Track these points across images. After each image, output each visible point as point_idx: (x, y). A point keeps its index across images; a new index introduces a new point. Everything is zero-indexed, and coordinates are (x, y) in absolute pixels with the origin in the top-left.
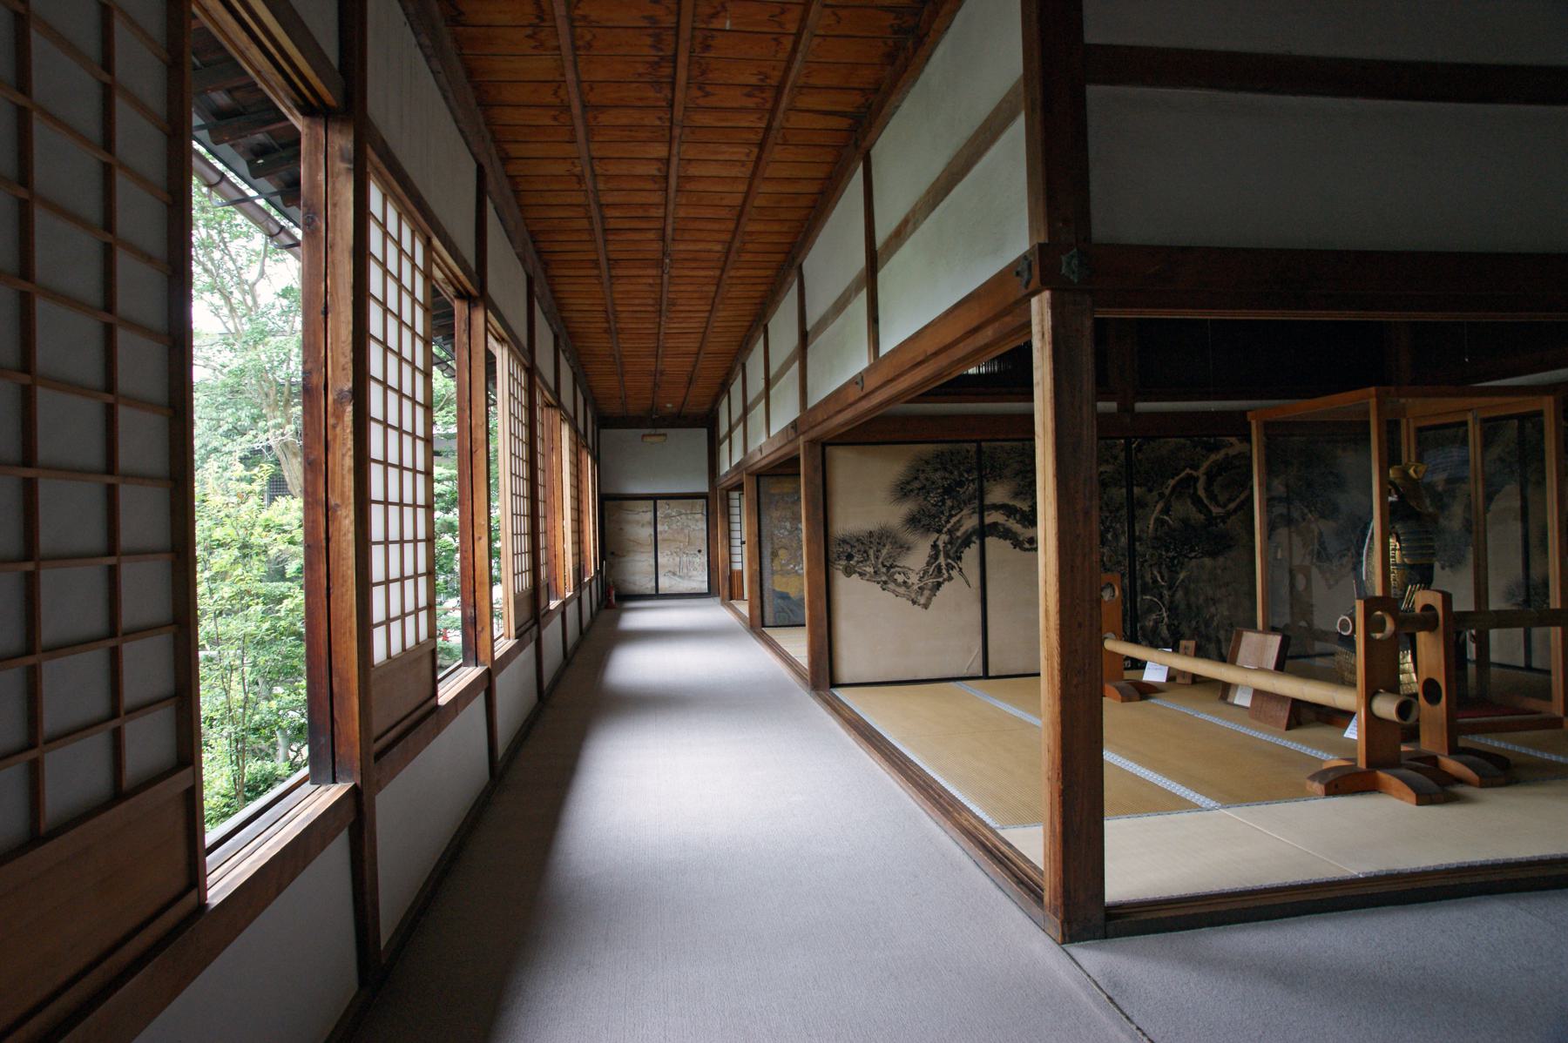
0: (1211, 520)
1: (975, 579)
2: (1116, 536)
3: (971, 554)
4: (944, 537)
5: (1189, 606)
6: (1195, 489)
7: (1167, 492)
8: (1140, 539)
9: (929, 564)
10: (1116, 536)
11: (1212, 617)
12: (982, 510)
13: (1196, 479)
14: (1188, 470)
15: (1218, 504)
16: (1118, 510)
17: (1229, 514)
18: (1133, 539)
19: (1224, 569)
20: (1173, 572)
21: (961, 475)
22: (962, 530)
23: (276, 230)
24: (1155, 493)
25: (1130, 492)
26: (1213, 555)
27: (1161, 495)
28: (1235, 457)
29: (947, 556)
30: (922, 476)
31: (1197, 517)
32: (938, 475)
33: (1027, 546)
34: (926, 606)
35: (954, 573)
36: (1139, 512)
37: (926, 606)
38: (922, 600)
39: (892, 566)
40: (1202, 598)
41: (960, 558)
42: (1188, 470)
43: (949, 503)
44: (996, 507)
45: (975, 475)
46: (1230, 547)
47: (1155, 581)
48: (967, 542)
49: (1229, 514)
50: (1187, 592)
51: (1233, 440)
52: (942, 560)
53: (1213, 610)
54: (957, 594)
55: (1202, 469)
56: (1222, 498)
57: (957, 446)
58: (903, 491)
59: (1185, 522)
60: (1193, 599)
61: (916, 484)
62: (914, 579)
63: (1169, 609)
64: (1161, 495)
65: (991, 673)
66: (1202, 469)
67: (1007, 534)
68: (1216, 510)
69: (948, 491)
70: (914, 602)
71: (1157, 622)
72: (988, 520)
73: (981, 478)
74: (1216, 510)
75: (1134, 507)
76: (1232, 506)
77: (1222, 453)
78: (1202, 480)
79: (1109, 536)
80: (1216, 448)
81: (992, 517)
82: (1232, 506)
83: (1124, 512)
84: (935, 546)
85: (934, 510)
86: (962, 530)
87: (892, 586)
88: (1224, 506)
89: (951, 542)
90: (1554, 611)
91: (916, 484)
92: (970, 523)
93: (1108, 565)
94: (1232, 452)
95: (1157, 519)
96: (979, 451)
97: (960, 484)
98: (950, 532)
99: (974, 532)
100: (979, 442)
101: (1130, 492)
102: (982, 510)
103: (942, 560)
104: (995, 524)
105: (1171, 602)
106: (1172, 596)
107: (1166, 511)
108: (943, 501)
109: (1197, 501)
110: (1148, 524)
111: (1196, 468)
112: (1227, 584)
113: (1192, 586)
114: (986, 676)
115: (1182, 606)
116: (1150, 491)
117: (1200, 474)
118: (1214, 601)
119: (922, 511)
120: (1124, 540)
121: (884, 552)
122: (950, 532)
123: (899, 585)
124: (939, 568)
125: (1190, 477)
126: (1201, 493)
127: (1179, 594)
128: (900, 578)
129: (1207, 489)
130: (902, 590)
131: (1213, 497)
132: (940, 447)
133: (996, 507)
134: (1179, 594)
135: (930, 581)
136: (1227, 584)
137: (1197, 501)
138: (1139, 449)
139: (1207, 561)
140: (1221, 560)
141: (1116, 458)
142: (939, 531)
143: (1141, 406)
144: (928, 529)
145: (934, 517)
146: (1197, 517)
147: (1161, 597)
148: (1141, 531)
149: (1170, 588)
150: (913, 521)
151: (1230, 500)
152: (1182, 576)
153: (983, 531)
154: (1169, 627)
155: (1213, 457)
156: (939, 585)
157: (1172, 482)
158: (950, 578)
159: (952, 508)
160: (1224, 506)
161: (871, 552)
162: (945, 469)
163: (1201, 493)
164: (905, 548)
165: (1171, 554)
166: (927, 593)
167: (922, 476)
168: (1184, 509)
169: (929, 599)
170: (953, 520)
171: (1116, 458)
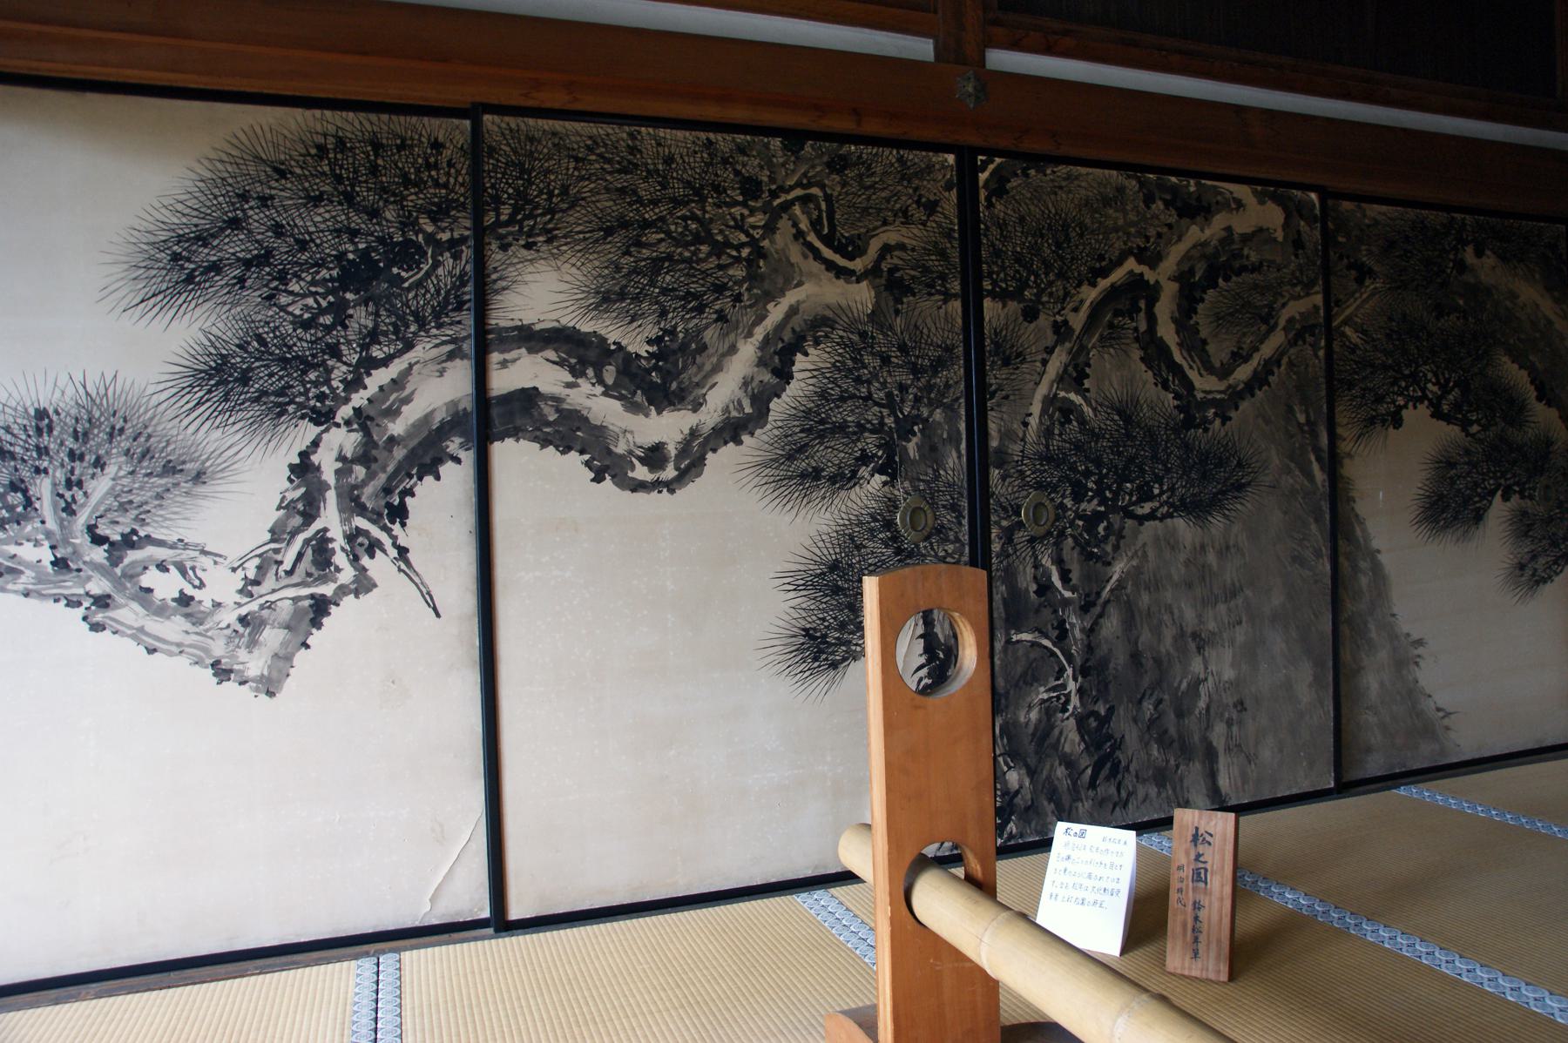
0: (1190, 411)
1: (459, 595)
2: (932, 451)
3: (441, 501)
4: (341, 440)
5: (1135, 657)
6: (1152, 319)
7: (1077, 321)
8: (1002, 459)
9: (276, 533)
10: (932, 451)
11: (1197, 683)
12: (484, 345)
13: (1152, 293)
14: (1131, 264)
15: (1208, 367)
16: (938, 365)
17: (1237, 395)
18: (980, 459)
19: (1224, 551)
20: (1094, 558)
21: (407, 223)
22: (411, 414)
23: (377, 352)
24: (1044, 321)
25: (973, 314)
26: (1197, 509)
27: (1061, 330)
28: (1246, 238)
29: (352, 503)
30: (258, 219)
31: (1158, 400)
32: (321, 218)
33: (641, 473)
34: (269, 686)
35: (380, 566)
36: (996, 376)
37: (269, 686)
38: (255, 664)
39: (130, 541)
40: (1169, 634)
41: (399, 513)
42: (1131, 264)
43: (361, 318)
44: (531, 338)
45: (463, 226)
46: (1240, 487)
47: (1045, 588)
48: (426, 457)
49: (1237, 395)
50: (1129, 622)
51: (1242, 191)
52: (331, 519)
53: (1197, 666)
54: (391, 639)
55: (1169, 265)
56: (1219, 352)
57: (400, 123)
58: (184, 263)
59: (1126, 412)
60: (1145, 637)
61: (235, 246)
62: (221, 586)
63: (1084, 671)
64: (1061, 330)
65: (515, 913)
66: (1169, 265)
67: (569, 432)
68: (1204, 384)
69: (358, 275)
70: (222, 672)
71: (1049, 711)
72: (503, 381)
73: (480, 234)
74: (1204, 384)
75: (983, 357)
76: (1243, 373)
77: (1219, 221)
78: (1170, 290)
79: (912, 447)
80: (1197, 210)
81: (518, 372)
82: (1243, 373)
83: (955, 373)
84: (303, 469)
85: (302, 344)
86: (411, 414)
87: (129, 613)
88: (1224, 372)
89: (366, 456)
90: (871, 573)
91: (235, 246)
92: (439, 389)
93: (909, 537)
94: (1242, 224)
95: (1049, 401)
96: (477, 147)
97: (408, 254)
98: (362, 420)
99: (454, 423)
100: (473, 112)
101: (973, 314)
102: (484, 345)
103: (331, 519)
104: (528, 398)
105: (1090, 648)
106: (1090, 632)
107: (1075, 376)
108: (340, 312)
109: (1156, 353)
110: (1026, 413)
111: (1151, 258)
112: (1232, 593)
113: (1145, 599)
114: (500, 923)
115: (1120, 659)
116: (1030, 314)
117: (1163, 274)
118: (1201, 642)
119: (256, 342)
120: (954, 462)
121: (100, 487)
122: (362, 420)
123: (161, 611)
124: (321, 547)
125: (1136, 282)
126: (1167, 332)
127: (1111, 625)
128: (166, 586)
129: (1183, 320)
130: (174, 628)
131: (1195, 345)
132: (333, 120)
133: (531, 338)
134: (1111, 625)
135: (286, 596)
136: (1232, 593)
137: (1156, 353)
138: (999, 187)
139: (1182, 526)
140: (1217, 522)
141: (932, 207)
142: (323, 418)
143: (1002, 59)
144: (278, 407)
145: (306, 365)
146: (1158, 400)
147: (1062, 635)
148: (1007, 435)
149: (1085, 608)
150: (222, 379)
151: (1239, 357)
152: (1118, 570)
153: (488, 421)
154: (1081, 721)
155: (1195, 234)
156: (321, 608)
157: (1090, 295)
158: (363, 585)
159: (373, 336)
160: (1224, 372)
161: (43, 489)
162: (349, 199)
163: (1167, 332)
164: (184, 473)
165: (1088, 507)
166: (272, 637)
167: (258, 219)
168: (1120, 375)
169: (283, 660)
170: (378, 379)
171: (932, 207)
